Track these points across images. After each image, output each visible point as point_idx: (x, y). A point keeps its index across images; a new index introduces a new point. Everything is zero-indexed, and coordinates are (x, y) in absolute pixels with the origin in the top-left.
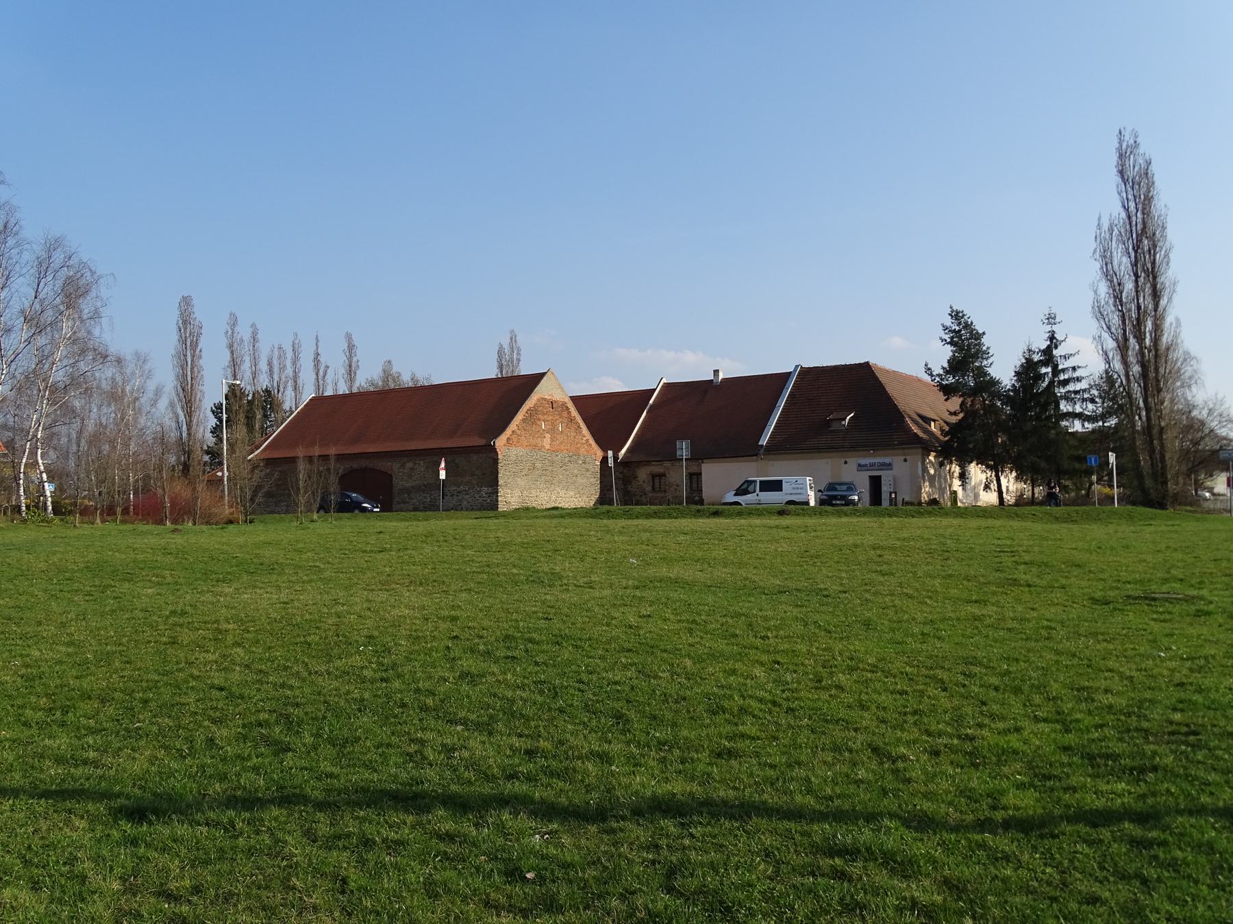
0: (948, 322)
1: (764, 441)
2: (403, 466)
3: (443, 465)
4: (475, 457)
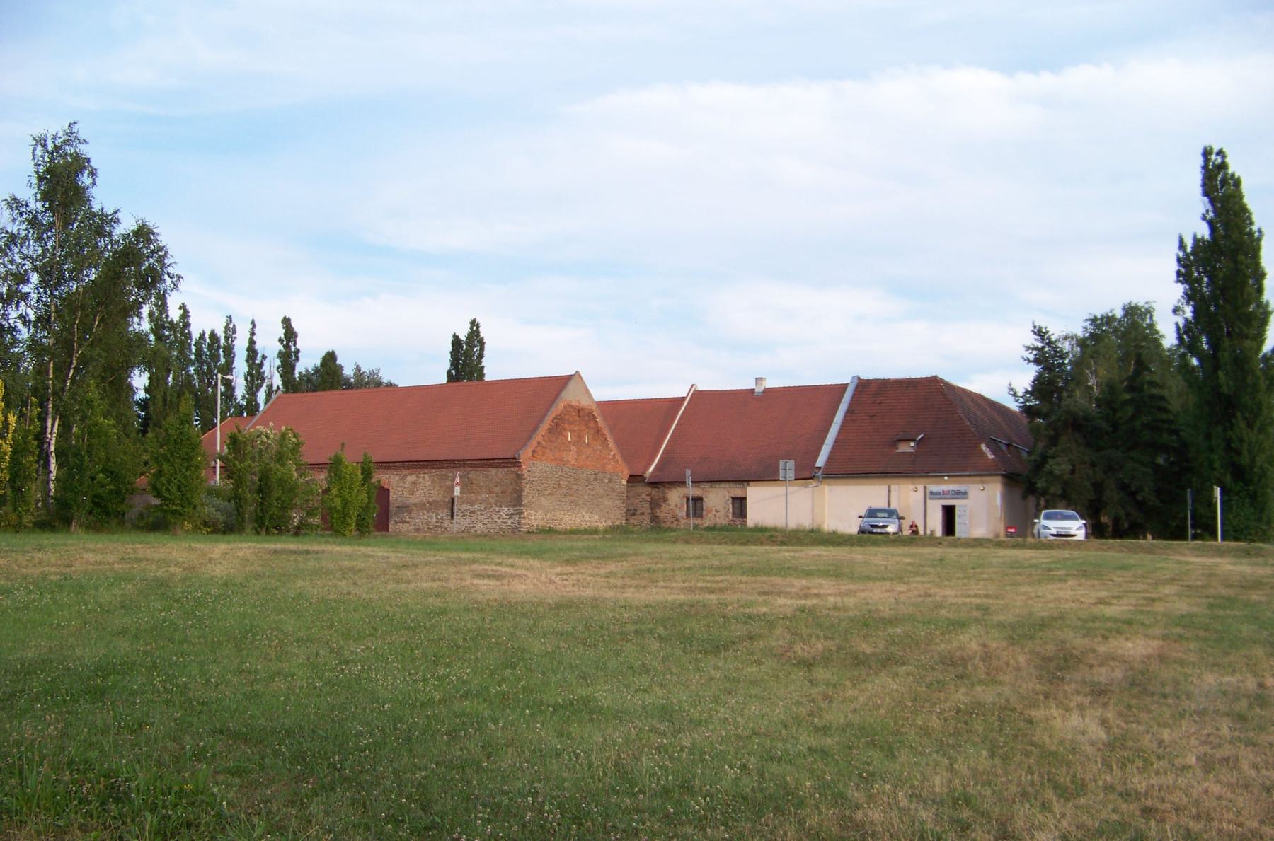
0: (1033, 341)
1: (821, 461)
2: (403, 479)
3: (458, 480)
4: (493, 471)
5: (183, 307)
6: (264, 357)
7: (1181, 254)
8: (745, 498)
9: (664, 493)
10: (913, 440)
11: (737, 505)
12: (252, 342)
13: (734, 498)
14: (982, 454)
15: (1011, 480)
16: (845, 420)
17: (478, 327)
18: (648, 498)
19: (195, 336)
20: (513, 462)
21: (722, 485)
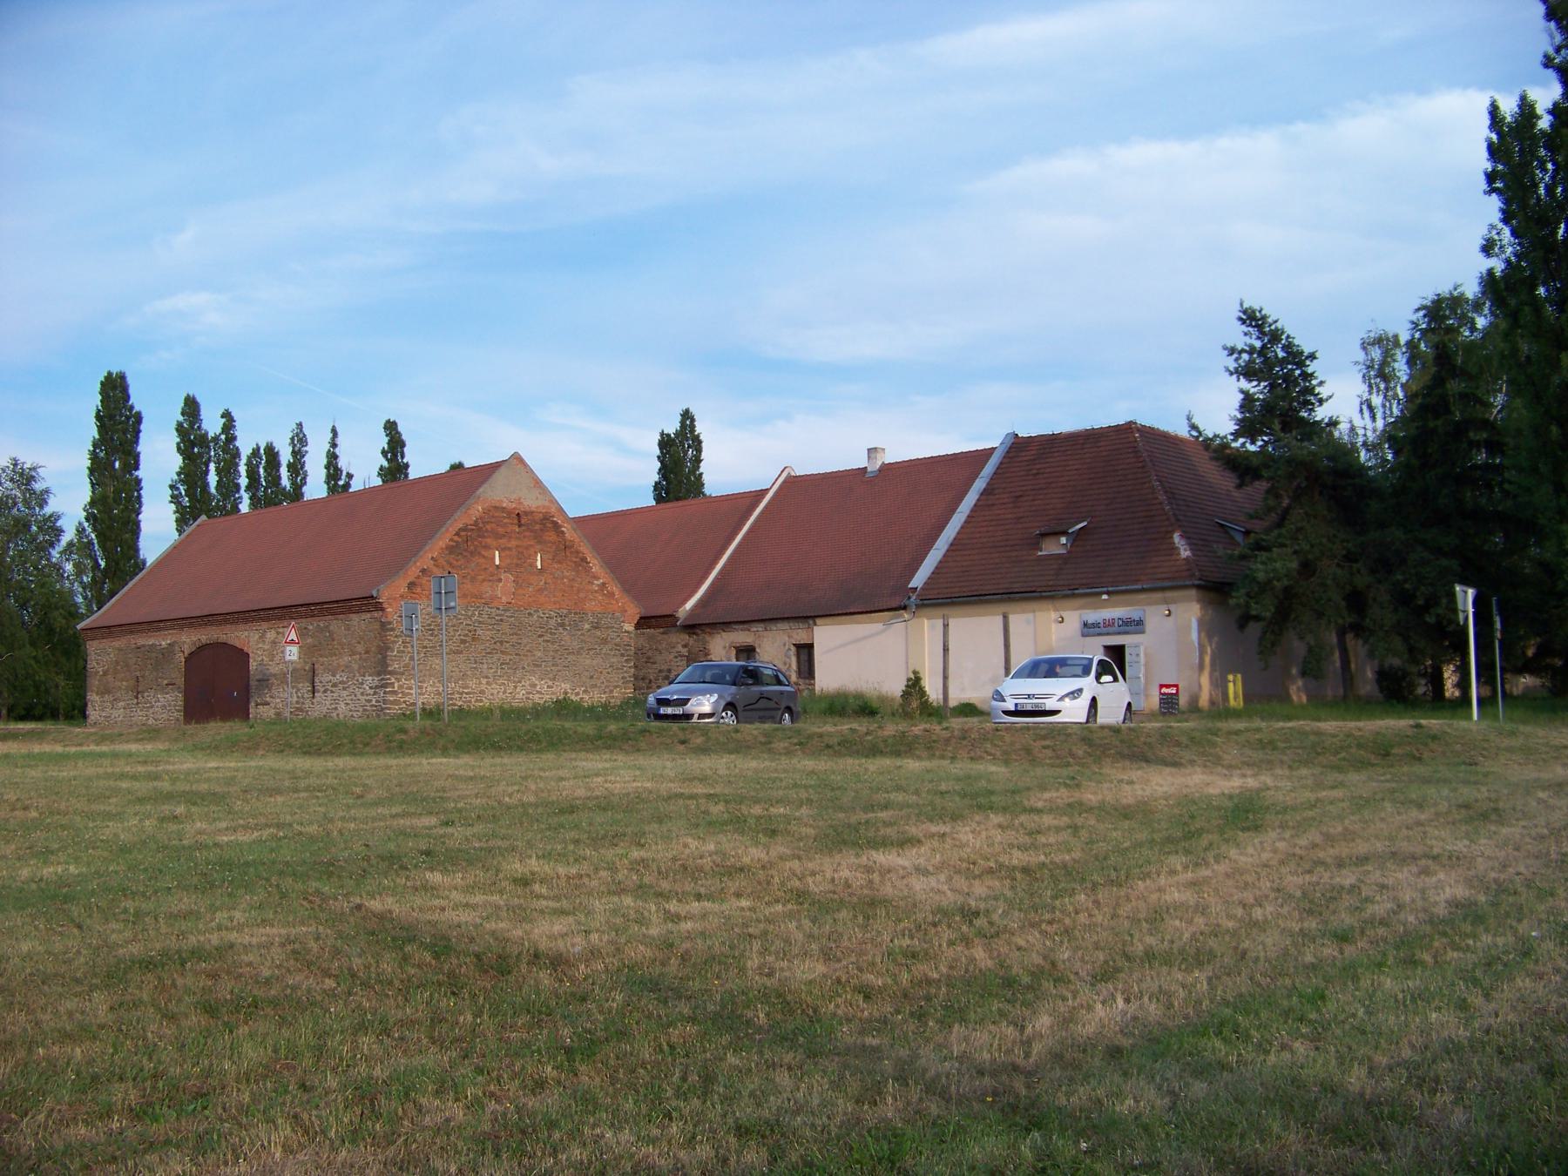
0: (1241, 337)
1: (919, 580)
5: (227, 415)
6: (350, 476)
7: (1494, 137)
8: (810, 647)
9: (705, 642)
10: (1064, 533)
11: (804, 657)
12: (332, 458)
13: (799, 647)
14: (1173, 549)
15: (1215, 590)
16: (976, 508)
17: (693, 420)
18: (685, 651)
19: (245, 452)
20: (369, 603)
21: (780, 625)
